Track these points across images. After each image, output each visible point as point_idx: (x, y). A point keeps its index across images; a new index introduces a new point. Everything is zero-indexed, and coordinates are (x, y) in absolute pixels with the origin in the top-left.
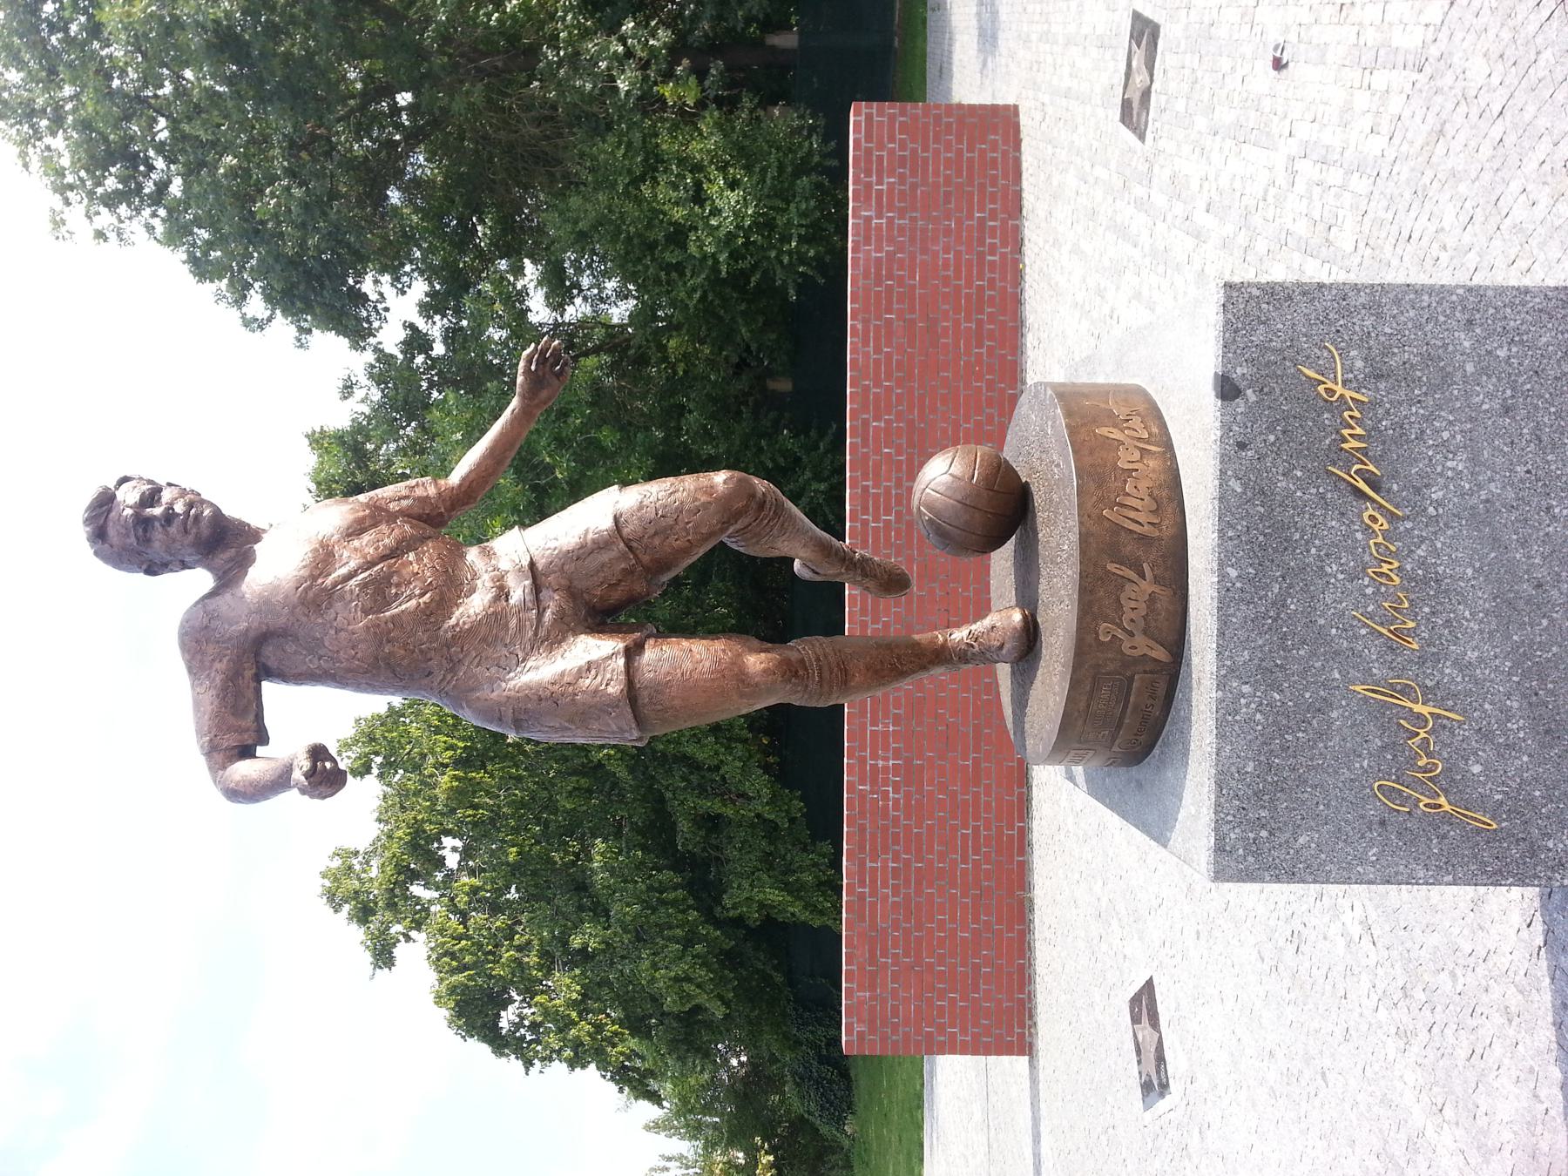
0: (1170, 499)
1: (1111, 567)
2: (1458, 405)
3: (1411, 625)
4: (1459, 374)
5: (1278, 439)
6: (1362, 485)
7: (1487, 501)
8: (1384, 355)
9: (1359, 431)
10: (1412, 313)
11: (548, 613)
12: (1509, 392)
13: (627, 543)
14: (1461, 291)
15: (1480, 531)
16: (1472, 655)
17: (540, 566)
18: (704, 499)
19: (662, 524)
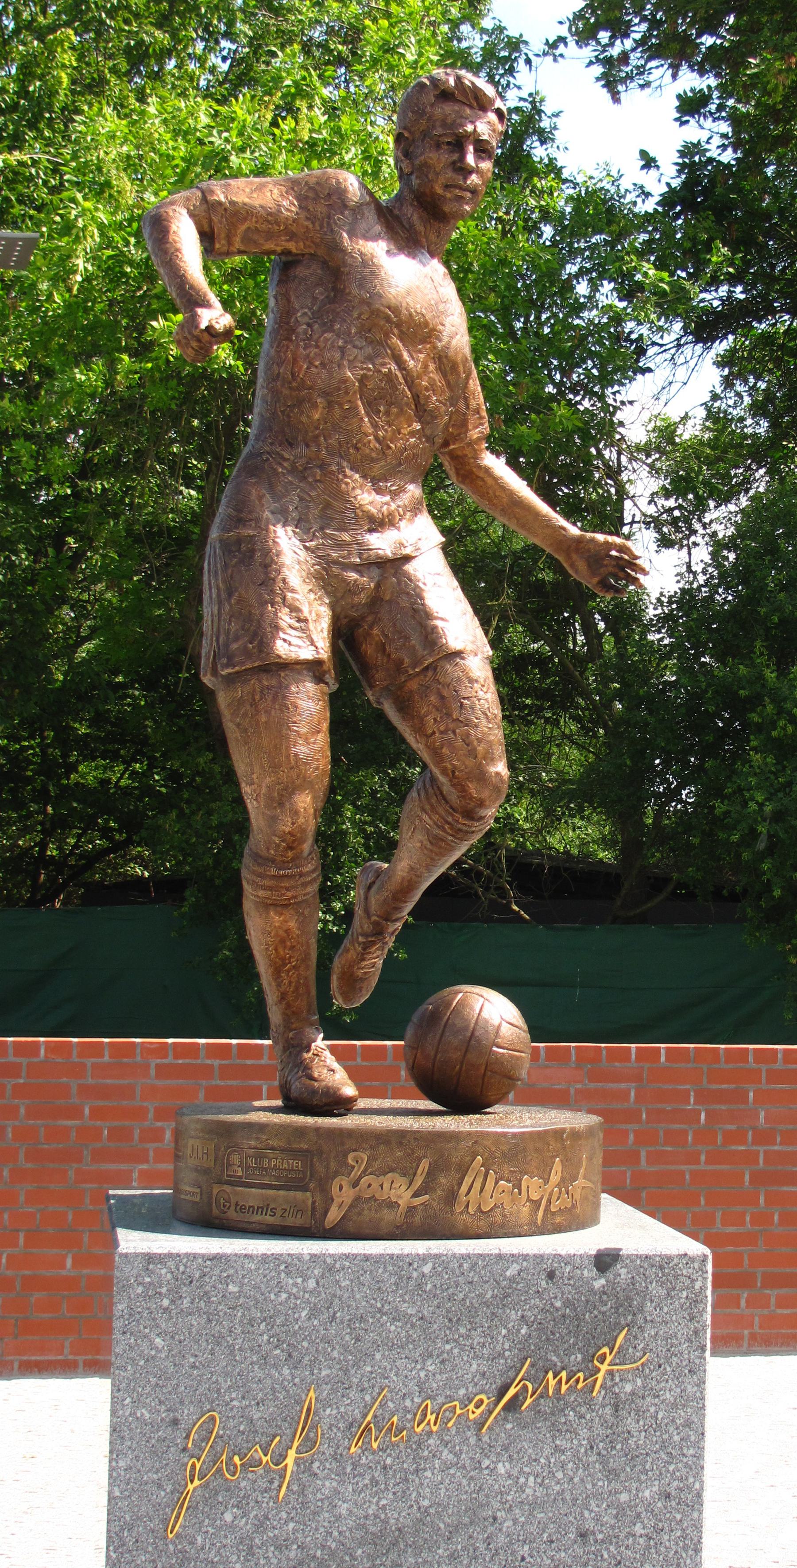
0: (492, 1225)
1: (424, 1165)
2: (589, 1486)
3: (375, 1445)
4: (618, 1486)
5: (557, 1310)
6: (512, 1392)
7: (495, 1519)
8: (637, 1412)
9: (564, 1388)
10: (676, 1438)
11: (353, 575)
12: (600, 1536)
13: (433, 667)
14: (697, 1486)
15: (466, 1511)
16: (343, 1508)
17: (409, 568)
18: (480, 748)
19: (451, 704)
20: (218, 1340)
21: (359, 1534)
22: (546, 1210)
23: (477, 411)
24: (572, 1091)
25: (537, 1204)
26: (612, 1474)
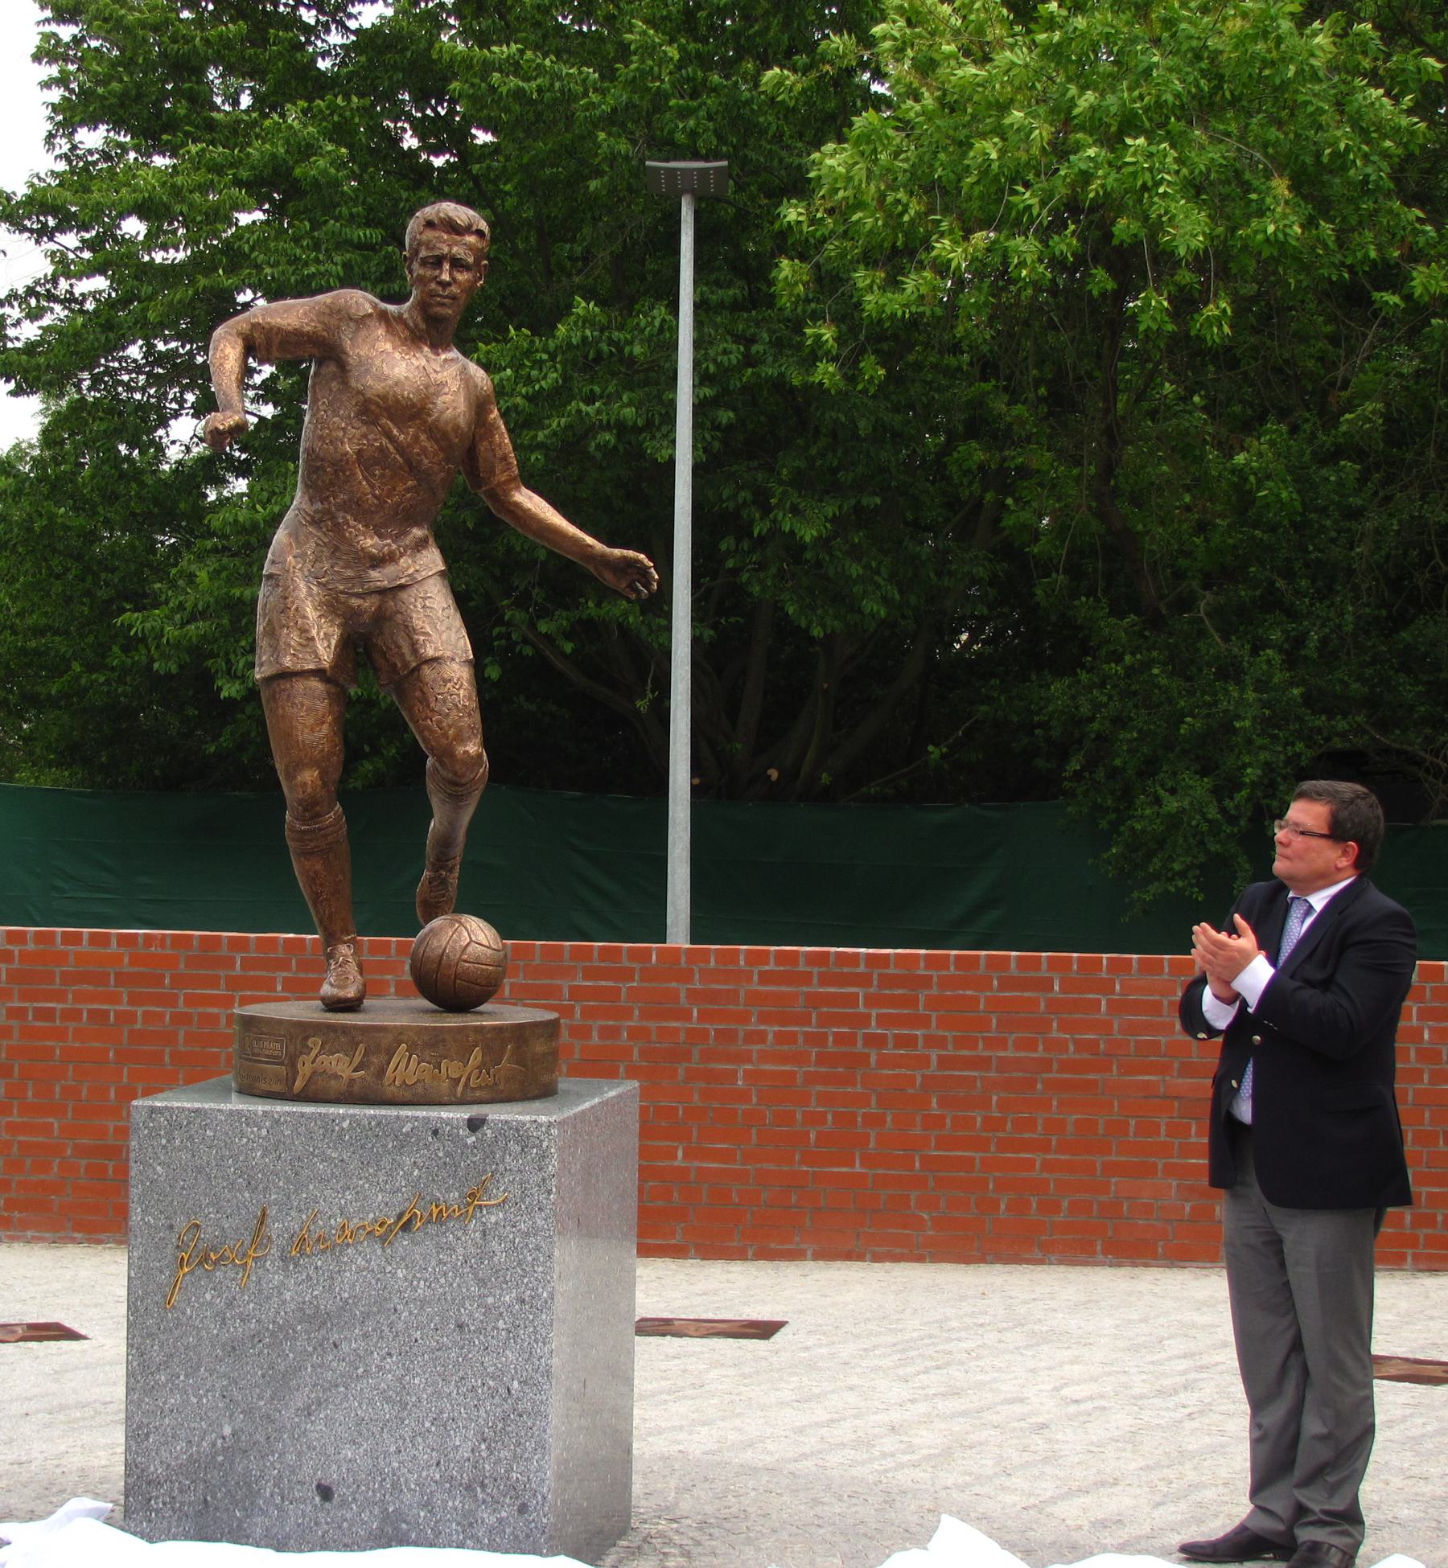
6: (405, 1219)
16: (288, 1296)
20: (199, 1170)
21: (298, 1315)
22: (466, 1085)
23: (505, 458)
24: (1165, 1003)
25: (457, 1081)
26: (482, 1283)
